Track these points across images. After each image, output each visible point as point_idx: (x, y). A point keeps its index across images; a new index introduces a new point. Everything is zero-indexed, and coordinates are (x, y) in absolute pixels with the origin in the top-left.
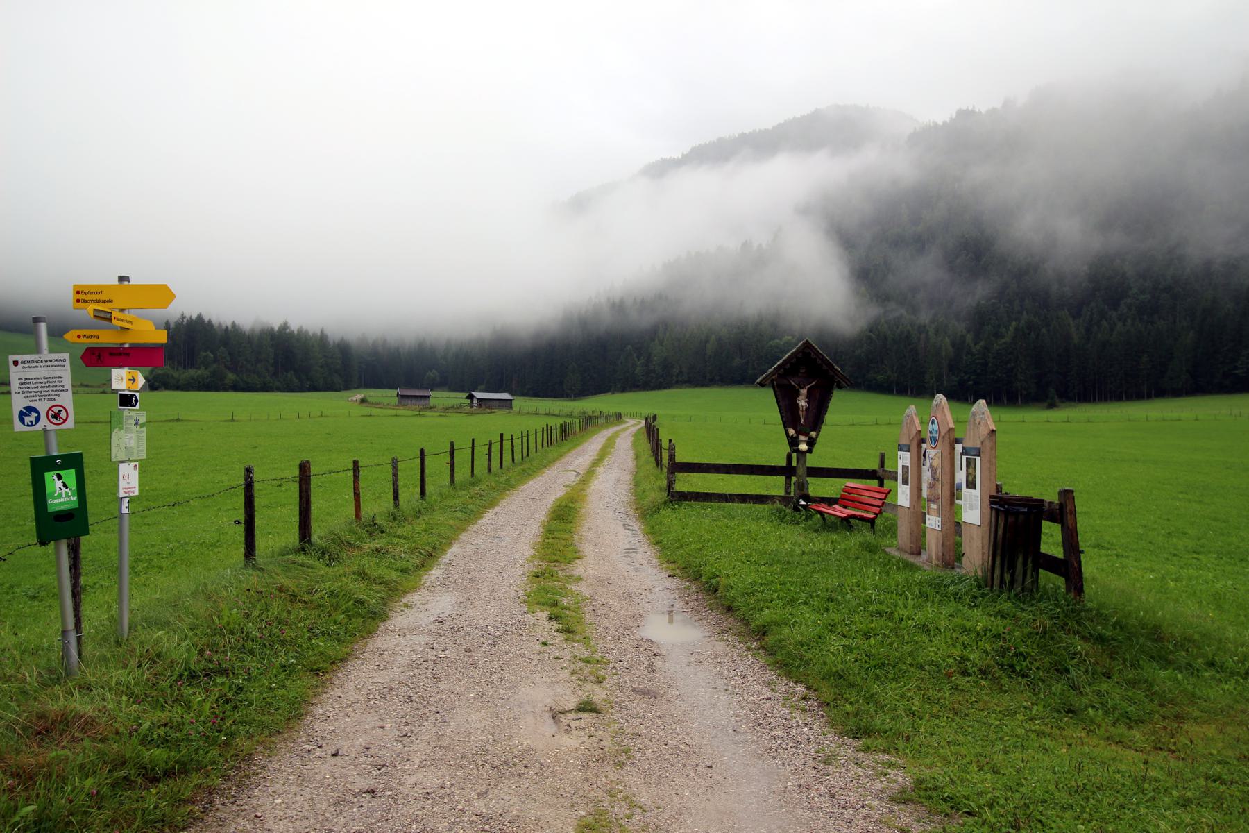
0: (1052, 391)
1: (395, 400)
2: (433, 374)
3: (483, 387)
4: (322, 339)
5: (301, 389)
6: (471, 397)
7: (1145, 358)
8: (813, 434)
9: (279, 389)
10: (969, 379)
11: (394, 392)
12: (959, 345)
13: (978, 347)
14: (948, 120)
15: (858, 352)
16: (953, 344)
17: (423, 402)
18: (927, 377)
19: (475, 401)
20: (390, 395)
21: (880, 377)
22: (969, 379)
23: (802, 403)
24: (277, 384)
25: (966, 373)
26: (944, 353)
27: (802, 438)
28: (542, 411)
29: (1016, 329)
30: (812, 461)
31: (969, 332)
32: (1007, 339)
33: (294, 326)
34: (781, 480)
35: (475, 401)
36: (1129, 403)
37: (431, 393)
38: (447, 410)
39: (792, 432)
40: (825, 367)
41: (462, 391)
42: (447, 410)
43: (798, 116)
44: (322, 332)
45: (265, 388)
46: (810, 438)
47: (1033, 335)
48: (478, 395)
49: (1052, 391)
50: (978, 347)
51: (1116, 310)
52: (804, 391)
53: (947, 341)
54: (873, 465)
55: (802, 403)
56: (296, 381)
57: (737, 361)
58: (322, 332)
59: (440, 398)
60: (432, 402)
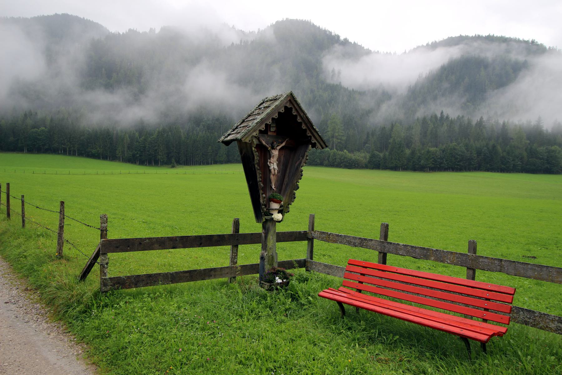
0: (173, 160)
7: (210, 148)
10: (137, 153)
14: (125, 33)
15: (82, 138)
18: (117, 152)
21: (94, 151)
22: (137, 153)
23: (274, 166)
25: (136, 150)
28: (470, 307)
32: (155, 136)
34: (227, 249)
36: (204, 166)
40: (304, 127)
43: (46, 15)
47: (165, 135)
49: (173, 160)
50: (141, 139)
51: (198, 127)
52: (275, 153)
54: (303, 227)
55: (274, 166)
57: (12, 139)
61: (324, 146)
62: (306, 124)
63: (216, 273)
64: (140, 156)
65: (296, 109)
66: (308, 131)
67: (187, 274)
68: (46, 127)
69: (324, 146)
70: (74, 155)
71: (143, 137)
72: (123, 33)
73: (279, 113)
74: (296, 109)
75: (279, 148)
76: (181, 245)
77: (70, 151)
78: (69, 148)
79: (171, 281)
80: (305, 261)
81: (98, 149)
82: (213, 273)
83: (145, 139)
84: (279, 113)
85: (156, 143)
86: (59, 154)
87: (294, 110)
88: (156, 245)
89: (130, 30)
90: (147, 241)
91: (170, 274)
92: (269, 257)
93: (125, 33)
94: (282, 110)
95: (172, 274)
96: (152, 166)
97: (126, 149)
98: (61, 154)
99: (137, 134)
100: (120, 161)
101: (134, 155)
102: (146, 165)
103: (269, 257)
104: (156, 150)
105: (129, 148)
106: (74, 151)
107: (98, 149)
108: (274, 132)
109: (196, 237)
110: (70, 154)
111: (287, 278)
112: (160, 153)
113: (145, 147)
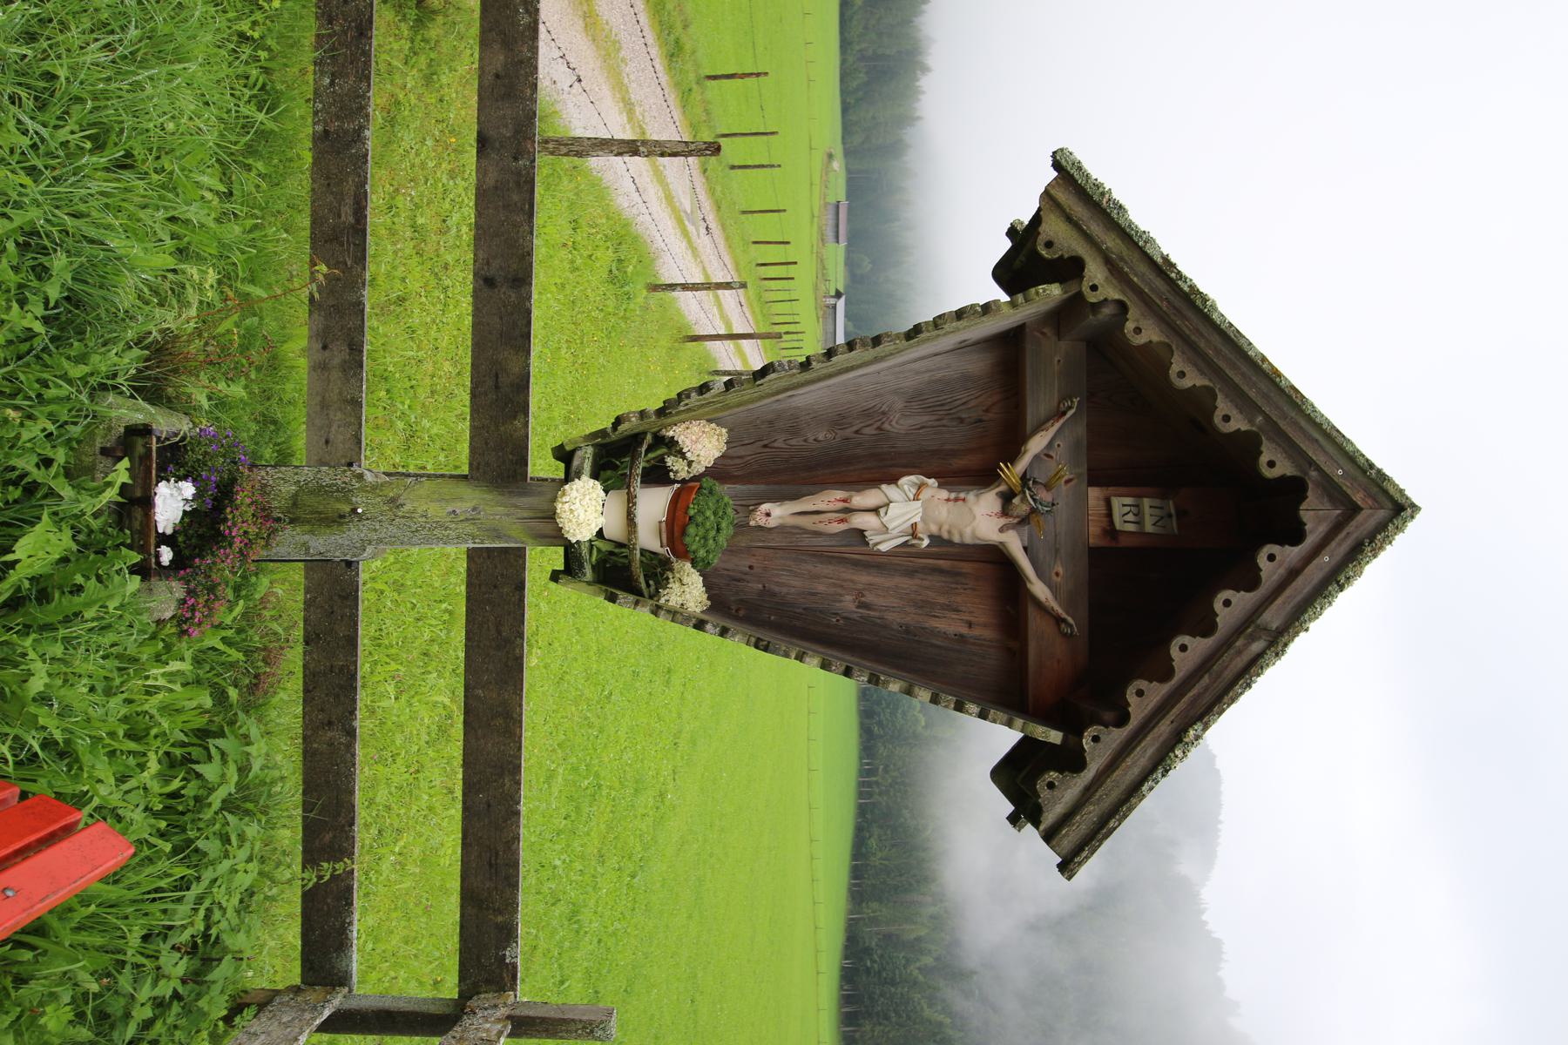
1: (832, 199)
2: (867, 266)
3: (851, 328)
4: (907, 119)
5: (844, 92)
6: (838, 295)
8: (688, 590)
9: (843, 62)
10: (874, 961)
11: (842, 196)
12: (916, 946)
13: (916, 972)
14: (1209, 927)
15: (905, 812)
16: (918, 939)
17: (830, 234)
18: (875, 905)
19: (832, 301)
20: (839, 192)
21: (873, 842)
24: (851, 59)
25: (882, 956)
26: (907, 927)
27: (653, 504)
29: (940, 1024)
30: (559, 617)
31: (937, 959)
32: (927, 1012)
33: (926, 83)
35: (832, 301)
37: (843, 244)
38: (821, 261)
39: (702, 445)
41: (846, 287)
42: (821, 261)
44: (919, 118)
45: (845, 44)
46: (658, 571)
48: (841, 304)
50: (916, 972)
52: (981, 518)
53: (923, 932)
55: (904, 511)
56: (855, 84)
58: (919, 118)
59: (836, 254)
60: (831, 246)
61: (1070, 836)
62: (1205, 665)
63: (336, 375)
64: (868, 971)
65: (1293, 574)
66: (1157, 692)
67: (347, 216)
68: (926, 727)
69: (1070, 836)
70: (861, 795)
71: (921, 978)
72: (1206, 923)
73: (1248, 444)
74: (1293, 574)
75: (1014, 544)
76: (490, 181)
77: (869, 784)
78: (877, 783)
79: (326, 132)
80: (341, 980)
81: (879, 855)
82: (339, 354)
83: (915, 983)
84: (1248, 444)
85: (909, 1018)
86: (861, 758)
87: (1290, 554)
88: (499, 60)
89: (1218, 943)
90: (525, 20)
91: (362, 128)
92: (345, 493)
93: (1204, 918)
94: (1274, 463)
95: (358, 136)
96: (841, 1006)
97: (884, 929)
98: (862, 765)
99: (928, 960)
100: (851, 913)
101: (867, 951)
102: (841, 988)
103: (345, 493)
104: (887, 1018)
105: (888, 937)
106: (870, 795)
107: (879, 855)
108: (1111, 531)
109: (526, 257)
110: (861, 784)
111: (178, 563)
112: (878, 1029)
113: (893, 983)
